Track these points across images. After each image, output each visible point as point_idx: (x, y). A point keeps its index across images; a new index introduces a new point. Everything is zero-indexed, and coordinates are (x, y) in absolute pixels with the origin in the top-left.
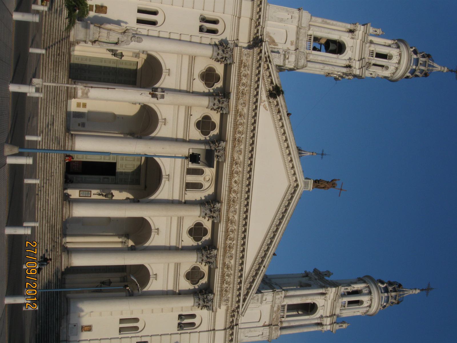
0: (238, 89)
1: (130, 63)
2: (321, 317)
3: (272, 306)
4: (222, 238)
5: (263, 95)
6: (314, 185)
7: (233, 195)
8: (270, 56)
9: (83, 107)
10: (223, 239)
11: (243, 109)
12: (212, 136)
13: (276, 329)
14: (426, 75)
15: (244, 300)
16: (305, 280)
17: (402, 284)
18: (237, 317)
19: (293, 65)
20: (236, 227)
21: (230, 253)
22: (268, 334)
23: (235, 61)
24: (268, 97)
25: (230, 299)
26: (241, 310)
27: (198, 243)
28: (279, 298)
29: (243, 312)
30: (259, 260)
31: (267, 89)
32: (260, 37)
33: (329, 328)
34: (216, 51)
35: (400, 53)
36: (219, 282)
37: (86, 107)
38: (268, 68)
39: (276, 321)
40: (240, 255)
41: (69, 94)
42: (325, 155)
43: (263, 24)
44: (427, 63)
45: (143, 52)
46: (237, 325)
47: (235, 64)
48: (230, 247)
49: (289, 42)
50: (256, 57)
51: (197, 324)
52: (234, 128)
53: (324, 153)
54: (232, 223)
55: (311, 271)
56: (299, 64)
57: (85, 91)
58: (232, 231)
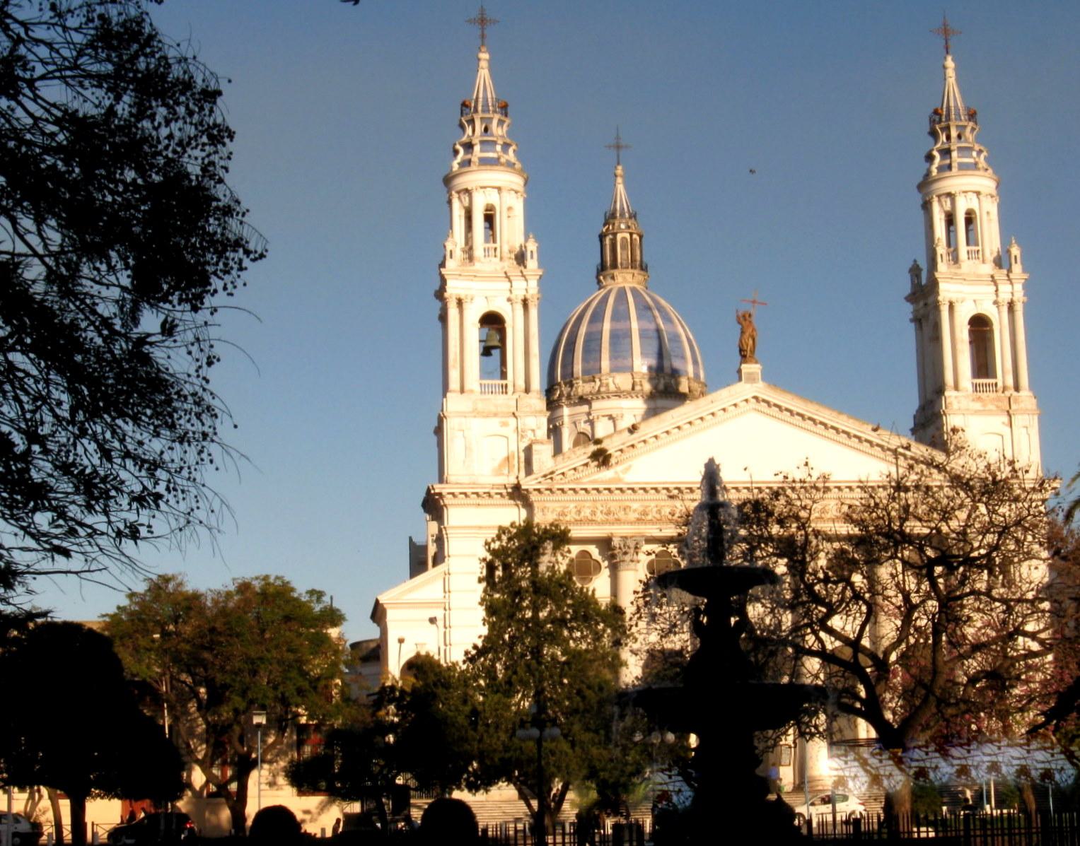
0: (603, 523)
5: (606, 474)
6: (751, 362)
11: (635, 511)
13: (1016, 401)
16: (927, 329)
22: (1026, 417)
32: (510, 490)
33: (1018, 287)
42: (618, 138)
49: (504, 431)
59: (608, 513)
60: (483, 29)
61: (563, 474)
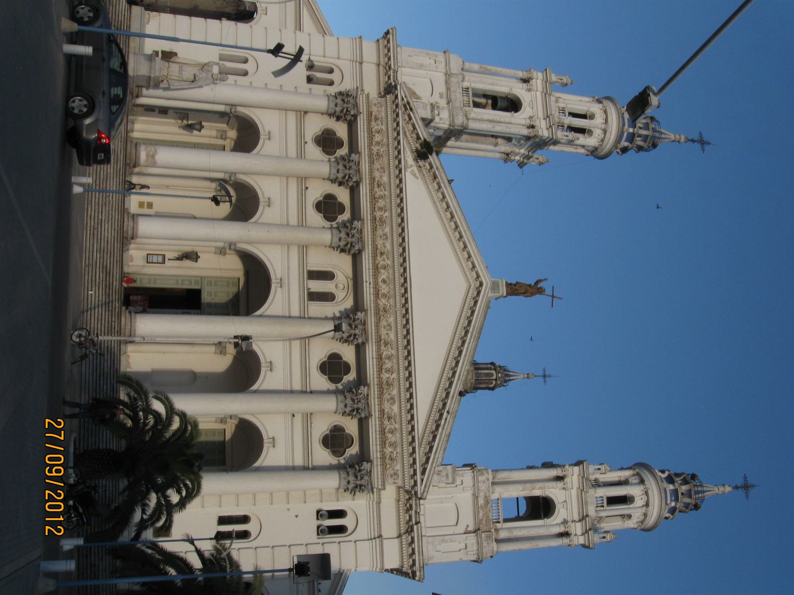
0: (370, 150)
1: (213, 432)
2: (565, 522)
3: (474, 495)
4: (373, 368)
5: (408, 158)
8: (411, 102)
9: (147, 208)
10: (375, 370)
12: (340, 222)
15: (423, 473)
17: (697, 474)
18: (416, 508)
19: (448, 123)
20: (393, 352)
21: (387, 321)
22: (475, 548)
23: (361, 111)
24: (417, 160)
25: (399, 472)
26: (420, 489)
27: (337, 387)
28: (483, 482)
29: (424, 491)
30: (438, 404)
31: (414, 148)
34: (345, 478)
35: (605, 109)
36: (378, 443)
37: (152, 208)
38: (410, 118)
39: (486, 525)
41: (128, 157)
42: (550, 376)
43: (395, 67)
45: (231, 417)
46: (417, 523)
47: (362, 115)
48: (388, 384)
51: (350, 528)
52: (371, 202)
53: (547, 373)
54: (386, 344)
56: (456, 121)
57: (151, 153)
58: (392, 432)
60: (741, 487)
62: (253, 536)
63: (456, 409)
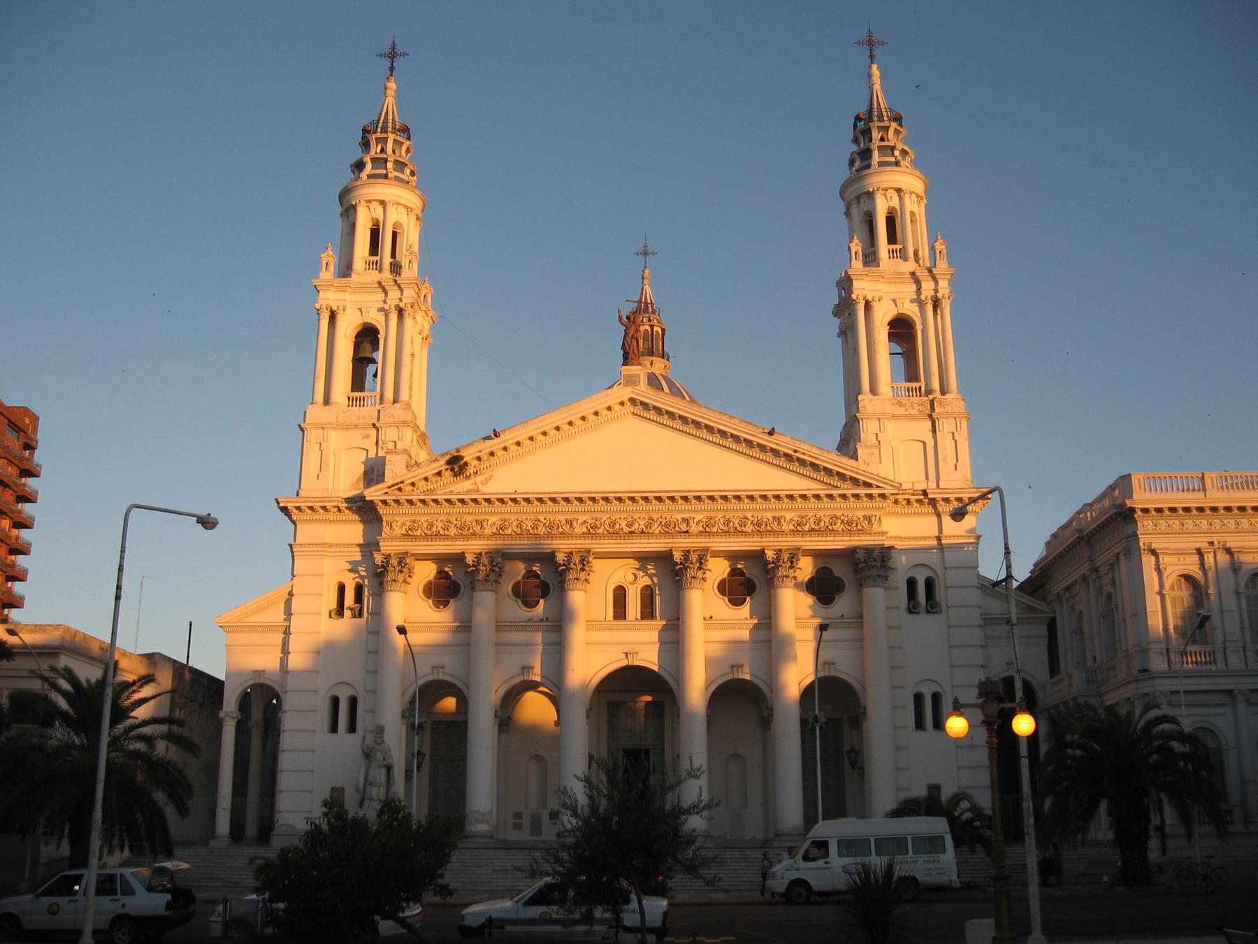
2: (921, 304)
5: (462, 487)
7: (656, 528)
14: (405, 130)
33: (944, 285)
40: (774, 504)
42: (646, 247)
44: (378, 135)
46: (925, 493)
50: (394, 509)
53: (641, 250)
55: (837, 321)
59: (759, 525)
61: (413, 484)
62: (938, 689)
63: (737, 422)
